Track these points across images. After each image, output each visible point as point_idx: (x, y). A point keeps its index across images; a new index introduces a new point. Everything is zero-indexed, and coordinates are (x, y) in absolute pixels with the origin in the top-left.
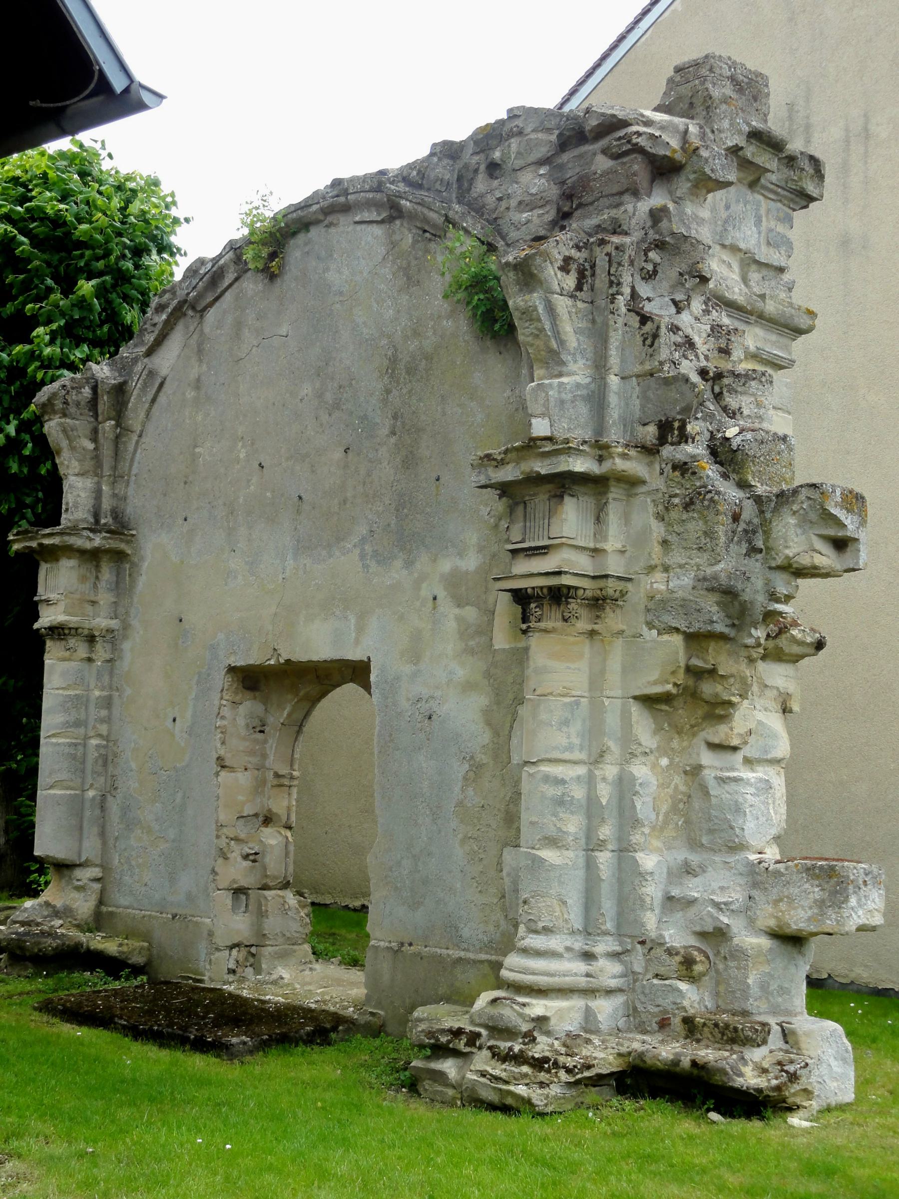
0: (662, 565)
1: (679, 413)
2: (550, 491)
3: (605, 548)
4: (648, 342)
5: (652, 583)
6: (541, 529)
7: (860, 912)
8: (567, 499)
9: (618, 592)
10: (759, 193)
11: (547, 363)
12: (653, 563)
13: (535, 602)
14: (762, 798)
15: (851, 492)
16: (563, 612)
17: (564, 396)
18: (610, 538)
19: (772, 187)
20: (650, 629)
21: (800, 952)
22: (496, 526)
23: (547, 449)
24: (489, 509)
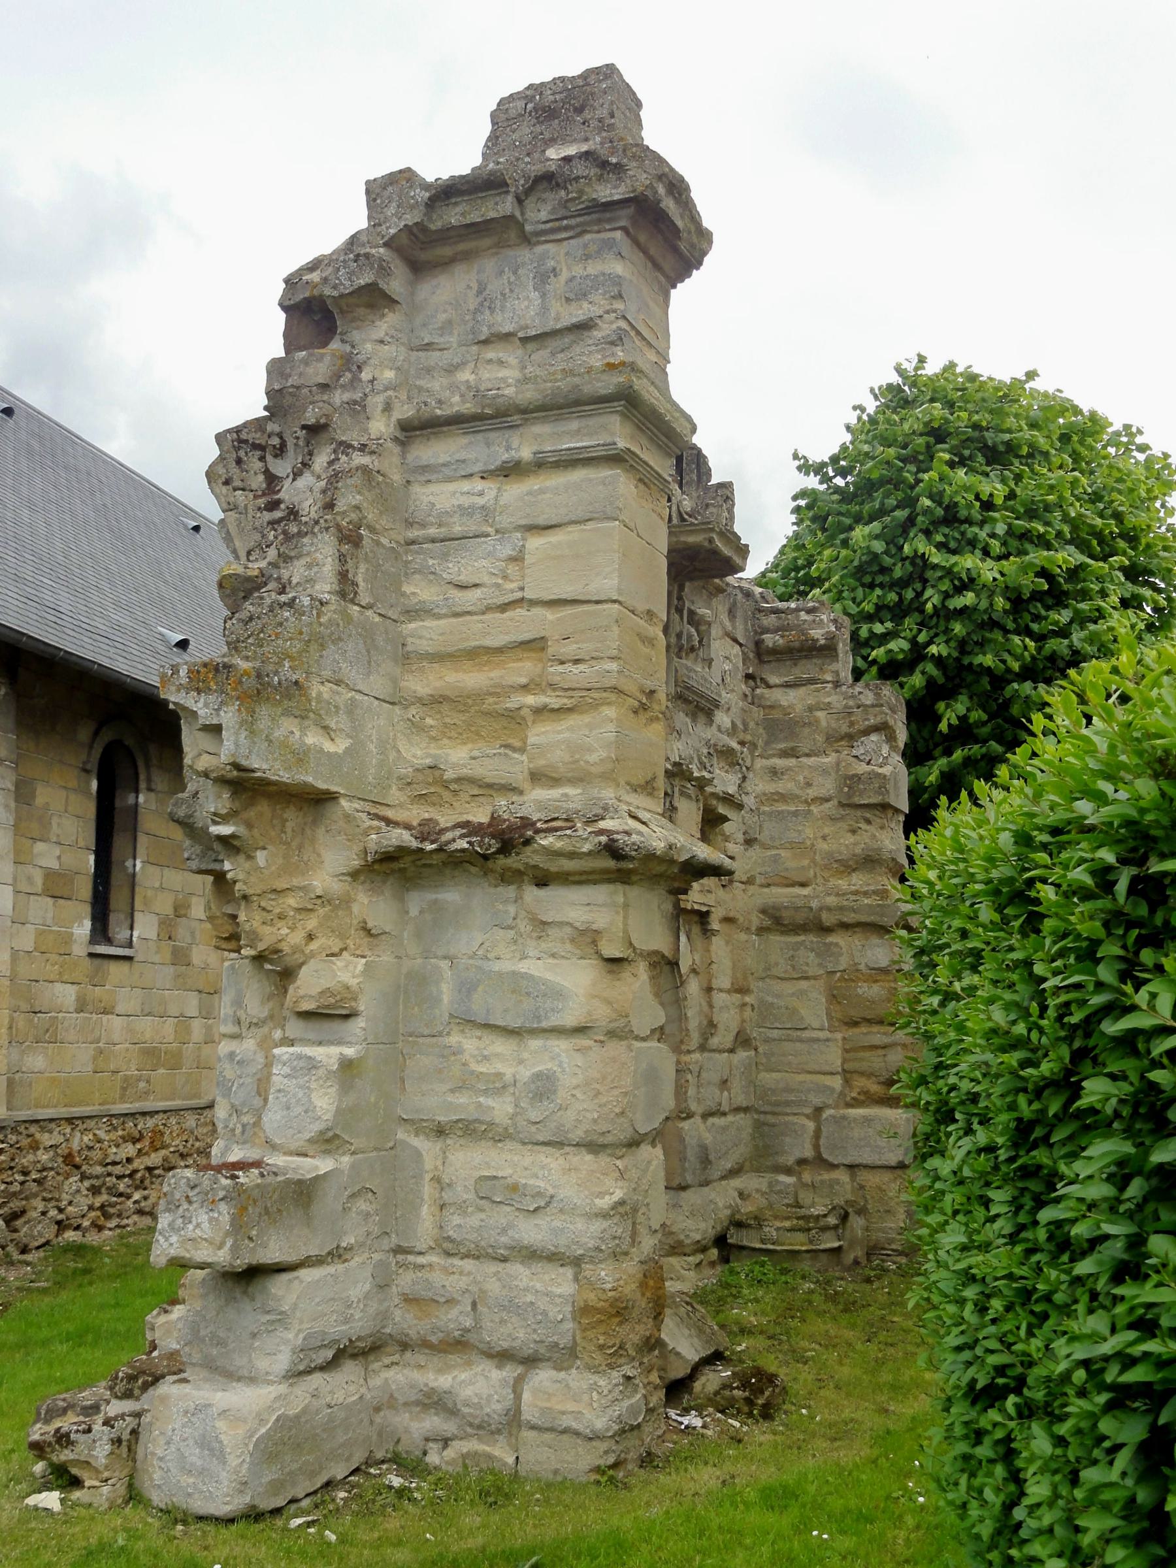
7: (174, 1239)
10: (539, 243)
14: (301, 1081)
15: (205, 665)
19: (549, 226)
21: (245, 1292)
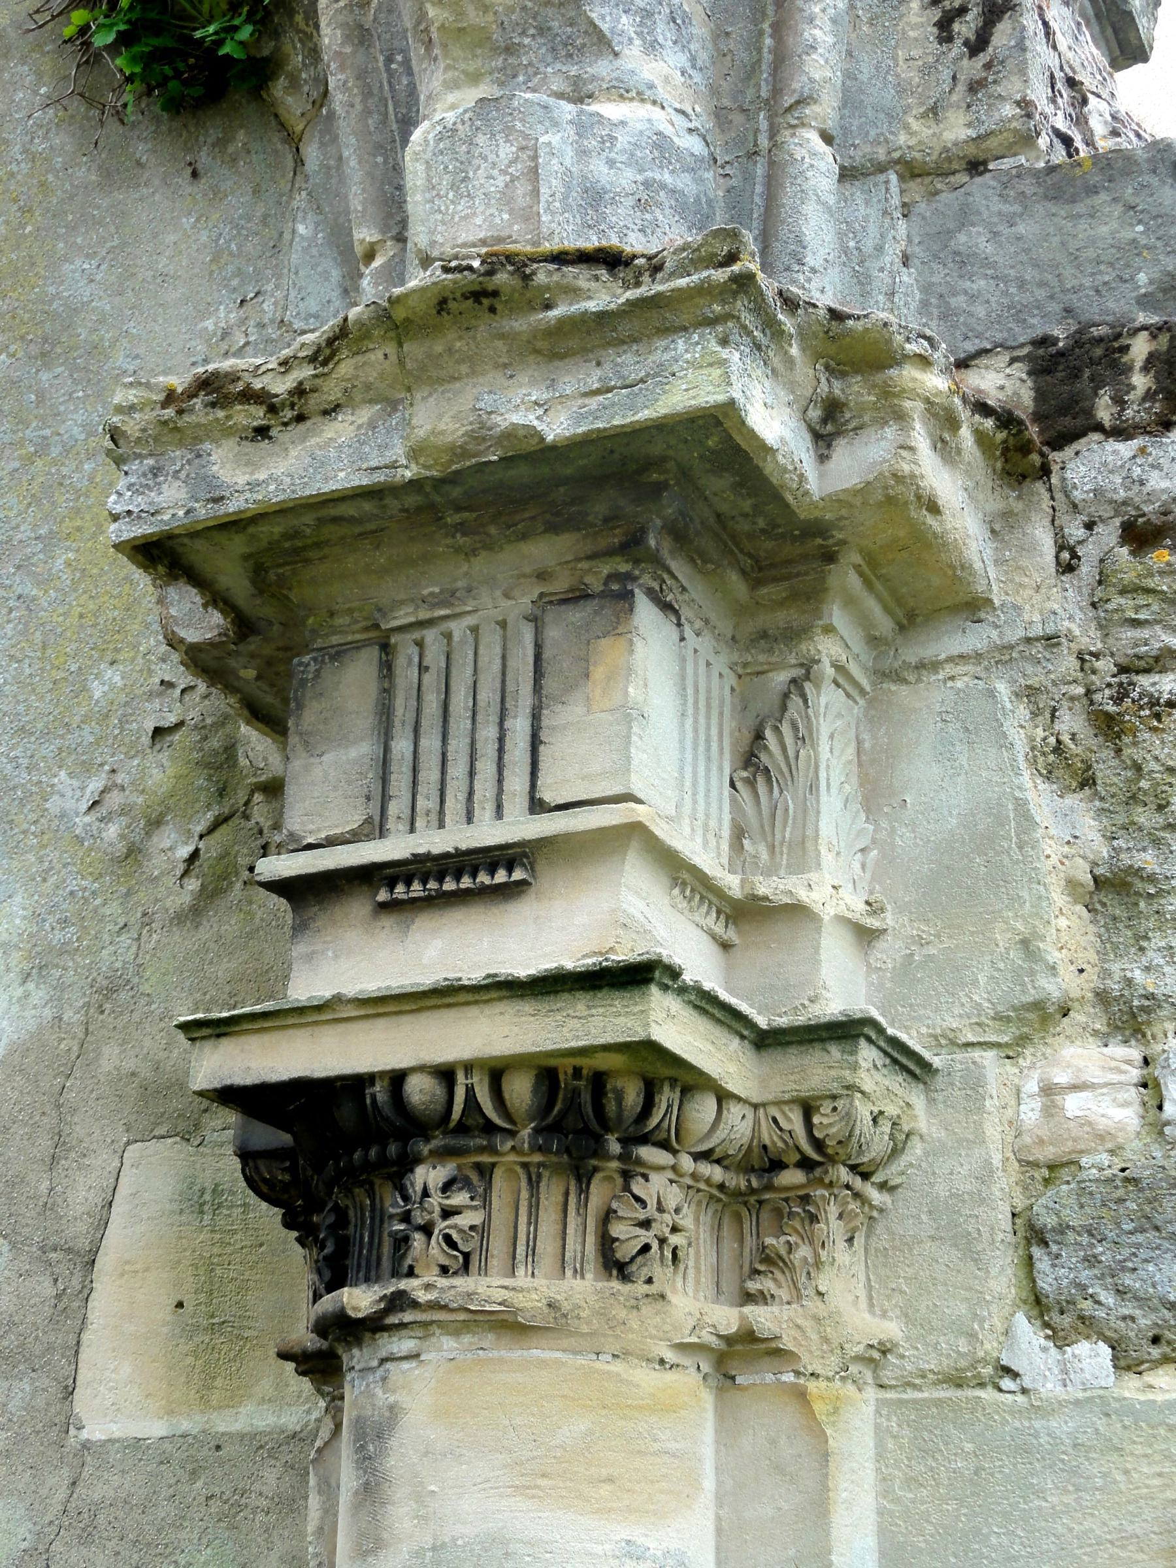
0: (1102, 997)
1: (1145, 302)
2: (542, 576)
3: (804, 895)
4: (965, 28)
5: (1048, 1090)
6: (486, 768)
8: (645, 612)
11: (510, 50)
12: (1052, 988)
16: (608, 1216)
17: (599, 169)
18: (827, 858)
20: (1059, 1339)
22: (133, 853)
23: (592, 306)
24: (95, 785)
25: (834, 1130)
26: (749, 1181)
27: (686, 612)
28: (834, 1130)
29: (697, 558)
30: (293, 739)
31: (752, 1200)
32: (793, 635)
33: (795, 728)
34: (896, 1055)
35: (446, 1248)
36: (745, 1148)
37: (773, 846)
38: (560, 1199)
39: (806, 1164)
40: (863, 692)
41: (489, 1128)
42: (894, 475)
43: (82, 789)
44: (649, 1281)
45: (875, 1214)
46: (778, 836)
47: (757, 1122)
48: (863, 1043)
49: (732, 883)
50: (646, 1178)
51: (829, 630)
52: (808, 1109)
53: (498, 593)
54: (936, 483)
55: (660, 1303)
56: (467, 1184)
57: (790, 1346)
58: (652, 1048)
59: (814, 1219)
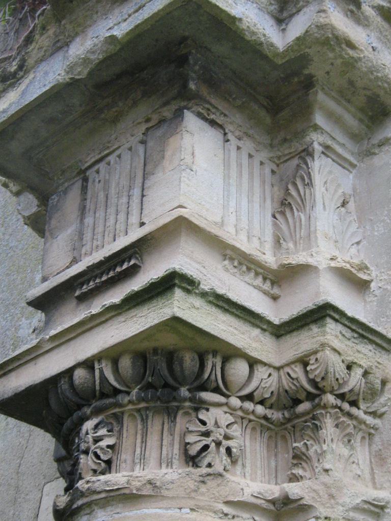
3: (311, 261)
6: (122, 217)
8: (191, 120)
9: (358, 373)
13: (97, 412)
25: (317, 372)
26: (283, 414)
27: (229, 128)
28: (317, 372)
29: (226, 96)
30: (47, 234)
31: (289, 426)
32: (300, 135)
33: (303, 179)
34: (360, 331)
35: (95, 460)
36: (276, 393)
37: (296, 242)
38: (160, 427)
39: (310, 397)
40: (354, 166)
41: (116, 392)
42: (317, 26)
43: (30, 323)
44: (209, 465)
45: (372, 431)
46: (298, 236)
47: (280, 377)
48: (329, 320)
49: (270, 259)
50: (208, 410)
51: (316, 128)
52: (305, 363)
53: (128, 135)
54: (345, 30)
55: (219, 480)
56: (107, 424)
57: (310, 502)
58: (176, 319)
59: (317, 428)
